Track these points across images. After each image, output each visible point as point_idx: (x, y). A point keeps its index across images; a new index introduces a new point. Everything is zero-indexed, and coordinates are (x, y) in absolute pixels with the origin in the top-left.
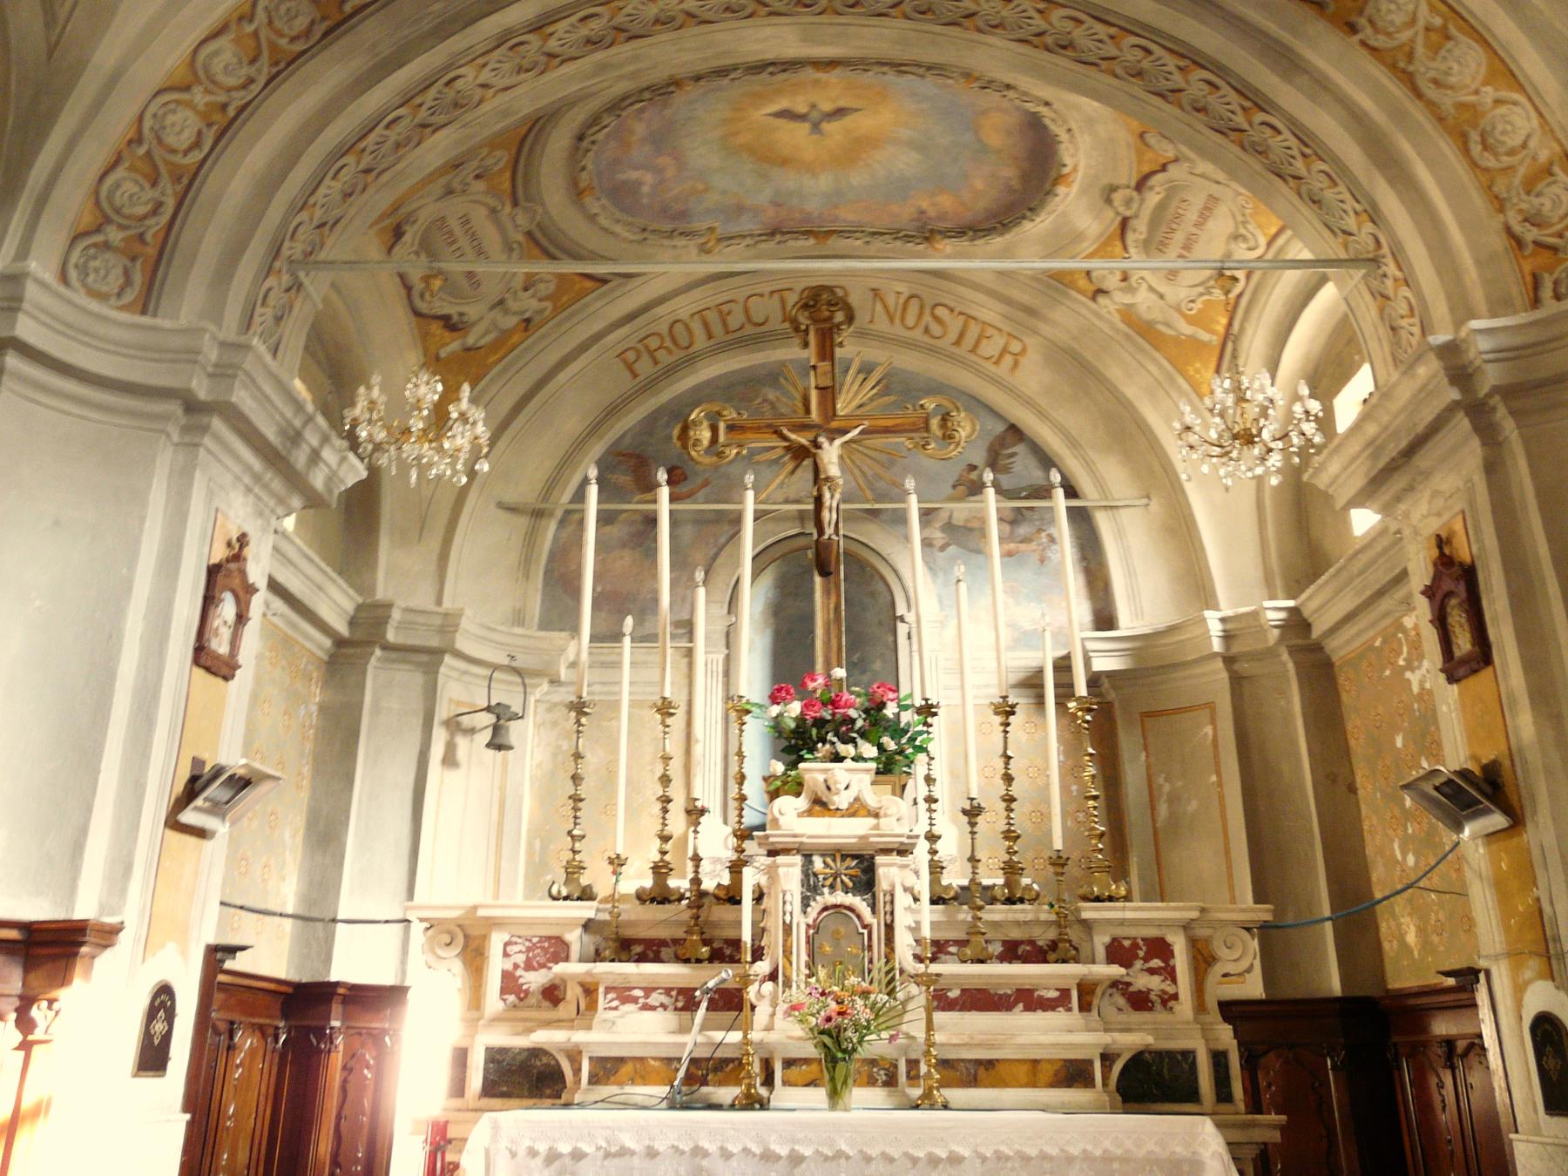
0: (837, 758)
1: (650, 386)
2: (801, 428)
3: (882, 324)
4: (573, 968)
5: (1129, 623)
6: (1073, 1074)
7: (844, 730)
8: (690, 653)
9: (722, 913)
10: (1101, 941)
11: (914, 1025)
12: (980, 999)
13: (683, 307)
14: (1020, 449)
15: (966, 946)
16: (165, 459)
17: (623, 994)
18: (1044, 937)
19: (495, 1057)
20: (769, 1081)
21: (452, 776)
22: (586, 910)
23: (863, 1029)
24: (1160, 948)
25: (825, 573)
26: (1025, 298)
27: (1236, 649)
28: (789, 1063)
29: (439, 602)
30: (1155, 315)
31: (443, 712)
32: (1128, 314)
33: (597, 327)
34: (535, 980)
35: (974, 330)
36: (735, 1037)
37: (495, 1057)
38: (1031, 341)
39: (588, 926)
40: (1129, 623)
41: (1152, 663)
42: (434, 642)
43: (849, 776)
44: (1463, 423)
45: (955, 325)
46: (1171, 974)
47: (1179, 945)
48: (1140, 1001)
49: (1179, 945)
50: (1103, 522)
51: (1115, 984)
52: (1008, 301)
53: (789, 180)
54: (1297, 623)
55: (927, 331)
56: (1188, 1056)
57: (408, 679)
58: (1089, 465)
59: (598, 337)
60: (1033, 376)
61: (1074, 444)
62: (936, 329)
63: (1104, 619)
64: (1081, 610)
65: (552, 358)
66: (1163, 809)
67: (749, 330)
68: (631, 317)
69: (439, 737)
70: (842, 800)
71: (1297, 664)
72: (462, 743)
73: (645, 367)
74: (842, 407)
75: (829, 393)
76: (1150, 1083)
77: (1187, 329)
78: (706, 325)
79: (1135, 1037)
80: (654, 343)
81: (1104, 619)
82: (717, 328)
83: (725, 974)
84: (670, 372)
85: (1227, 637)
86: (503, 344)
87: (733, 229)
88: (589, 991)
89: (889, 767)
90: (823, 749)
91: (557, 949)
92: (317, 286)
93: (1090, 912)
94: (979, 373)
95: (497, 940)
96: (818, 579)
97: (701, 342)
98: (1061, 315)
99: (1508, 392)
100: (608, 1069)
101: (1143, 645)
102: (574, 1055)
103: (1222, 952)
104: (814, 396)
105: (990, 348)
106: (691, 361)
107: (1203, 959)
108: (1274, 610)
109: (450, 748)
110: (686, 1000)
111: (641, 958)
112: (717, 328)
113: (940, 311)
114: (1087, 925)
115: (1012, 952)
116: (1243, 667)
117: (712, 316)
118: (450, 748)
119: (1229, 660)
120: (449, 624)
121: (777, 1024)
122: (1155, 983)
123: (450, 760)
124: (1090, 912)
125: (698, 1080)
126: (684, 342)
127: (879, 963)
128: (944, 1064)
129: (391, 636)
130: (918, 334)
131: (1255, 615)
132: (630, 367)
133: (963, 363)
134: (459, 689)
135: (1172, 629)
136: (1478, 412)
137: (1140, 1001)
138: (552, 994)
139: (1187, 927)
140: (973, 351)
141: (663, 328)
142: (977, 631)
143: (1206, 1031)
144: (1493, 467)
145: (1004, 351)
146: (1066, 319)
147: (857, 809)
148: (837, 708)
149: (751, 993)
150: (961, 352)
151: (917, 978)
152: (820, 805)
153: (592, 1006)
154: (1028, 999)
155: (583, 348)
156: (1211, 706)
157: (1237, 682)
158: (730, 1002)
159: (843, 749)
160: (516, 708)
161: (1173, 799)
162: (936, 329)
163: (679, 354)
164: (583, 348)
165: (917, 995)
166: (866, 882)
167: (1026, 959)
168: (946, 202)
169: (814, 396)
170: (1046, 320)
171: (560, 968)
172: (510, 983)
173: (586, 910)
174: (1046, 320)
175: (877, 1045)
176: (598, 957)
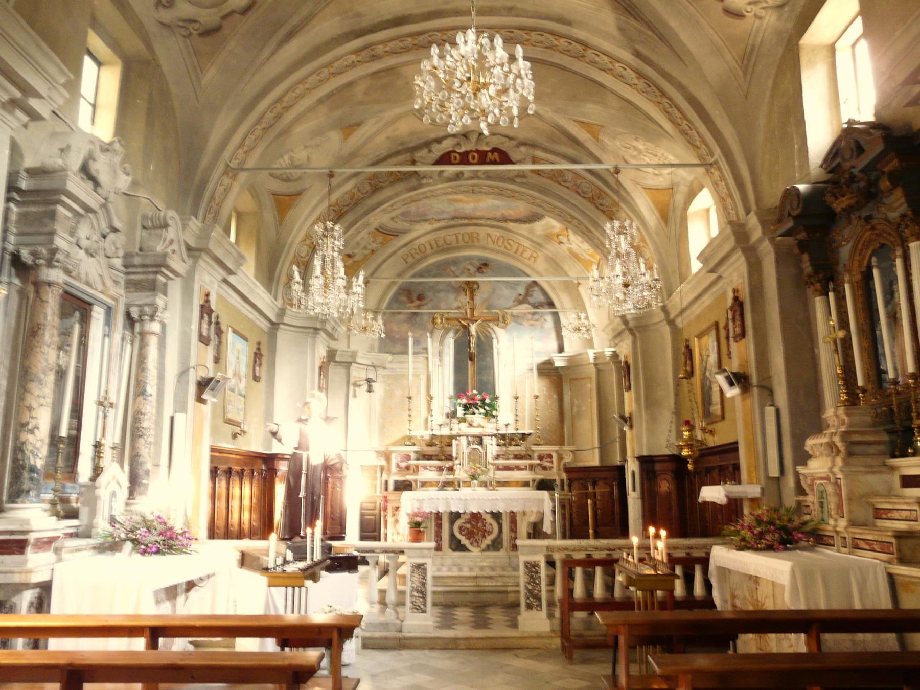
0: (474, 413)
1: (412, 266)
2: (465, 319)
3: (491, 245)
4: (413, 462)
5: (569, 350)
6: (526, 484)
7: (476, 406)
8: (427, 358)
9: (448, 448)
10: (536, 455)
11: (491, 474)
12: (507, 468)
13: (423, 240)
14: (536, 289)
15: (505, 456)
16: (310, 340)
17: (425, 468)
18: (523, 453)
19: (396, 482)
20: (459, 486)
21: (356, 400)
22: (415, 448)
23: (479, 475)
24: (550, 456)
25: (471, 360)
26: (538, 241)
27: (598, 362)
28: (464, 482)
29: (348, 347)
30: (577, 252)
31: (352, 380)
32: (570, 250)
33: (394, 249)
34: (403, 465)
35: (521, 249)
36: (451, 477)
37: (396, 482)
38: (540, 254)
39: (416, 452)
40: (569, 350)
41: (574, 363)
42: (349, 360)
43: (478, 418)
44: (627, 332)
45: (515, 246)
46: (552, 462)
47: (554, 455)
48: (545, 468)
49: (554, 455)
50: (561, 316)
51: (539, 464)
52: (532, 241)
53: (459, 205)
54: (615, 355)
55: (505, 248)
56: (554, 481)
57: (341, 371)
58: (558, 297)
59: (395, 252)
60: (541, 265)
61: (553, 288)
62: (509, 247)
63: (561, 349)
64: (554, 345)
65: (380, 260)
66: (575, 409)
67: (446, 246)
68: (406, 245)
69: (351, 388)
70: (475, 424)
71: (777, 248)
72: (357, 389)
73: (410, 260)
74: (476, 314)
75: (472, 310)
76: (543, 485)
77: (588, 257)
78: (431, 245)
79: (540, 476)
80: (413, 252)
81: (561, 349)
82: (434, 246)
83: (448, 464)
84: (419, 261)
85: (596, 358)
86: (366, 258)
87: (441, 217)
88: (417, 467)
89: (489, 415)
90: (471, 410)
91: (408, 458)
92: (445, 432)
93: (534, 448)
94: (523, 263)
95: (393, 456)
96: (469, 362)
97: (429, 251)
98: (548, 246)
99: (637, 327)
100: (424, 484)
101: (571, 359)
102: (416, 481)
103: (566, 457)
104: (468, 311)
105: (527, 255)
106: (426, 257)
107: (560, 458)
108: (608, 351)
109: (355, 391)
110: (440, 469)
111: (428, 459)
112: (434, 246)
113: (511, 242)
114: (533, 451)
115: (516, 457)
116: (600, 367)
117: (433, 243)
118: (355, 391)
119: (596, 365)
120: (354, 354)
121: (461, 474)
122: (548, 464)
123: (355, 396)
124: (534, 448)
125: (446, 485)
126: (423, 250)
127: (483, 460)
128: (498, 482)
129: (337, 359)
130: (502, 249)
131: (603, 352)
132: (405, 260)
133: (518, 260)
134: (357, 373)
135: (579, 354)
136: (631, 331)
137: (545, 468)
138: (408, 468)
139: (556, 451)
140: (521, 255)
141: (416, 247)
142: (518, 355)
143: (559, 475)
144: (634, 343)
145: (531, 256)
146: (552, 247)
147: (480, 426)
148: (474, 381)
149: (455, 467)
150: (517, 255)
151: (493, 464)
152: (471, 425)
153: (418, 470)
154: (518, 468)
155: (390, 256)
156: (590, 378)
157: (599, 371)
158: (451, 469)
159: (476, 411)
160: (374, 379)
161: (579, 406)
162: (509, 247)
163: (422, 255)
164: (390, 256)
165: (491, 467)
166: (481, 443)
167: (518, 459)
168: (511, 212)
169: (468, 311)
170: (546, 249)
171: (410, 462)
172: (398, 466)
173: (415, 448)
174: (546, 249)
175: (483, 478)
176: (418, 459)
